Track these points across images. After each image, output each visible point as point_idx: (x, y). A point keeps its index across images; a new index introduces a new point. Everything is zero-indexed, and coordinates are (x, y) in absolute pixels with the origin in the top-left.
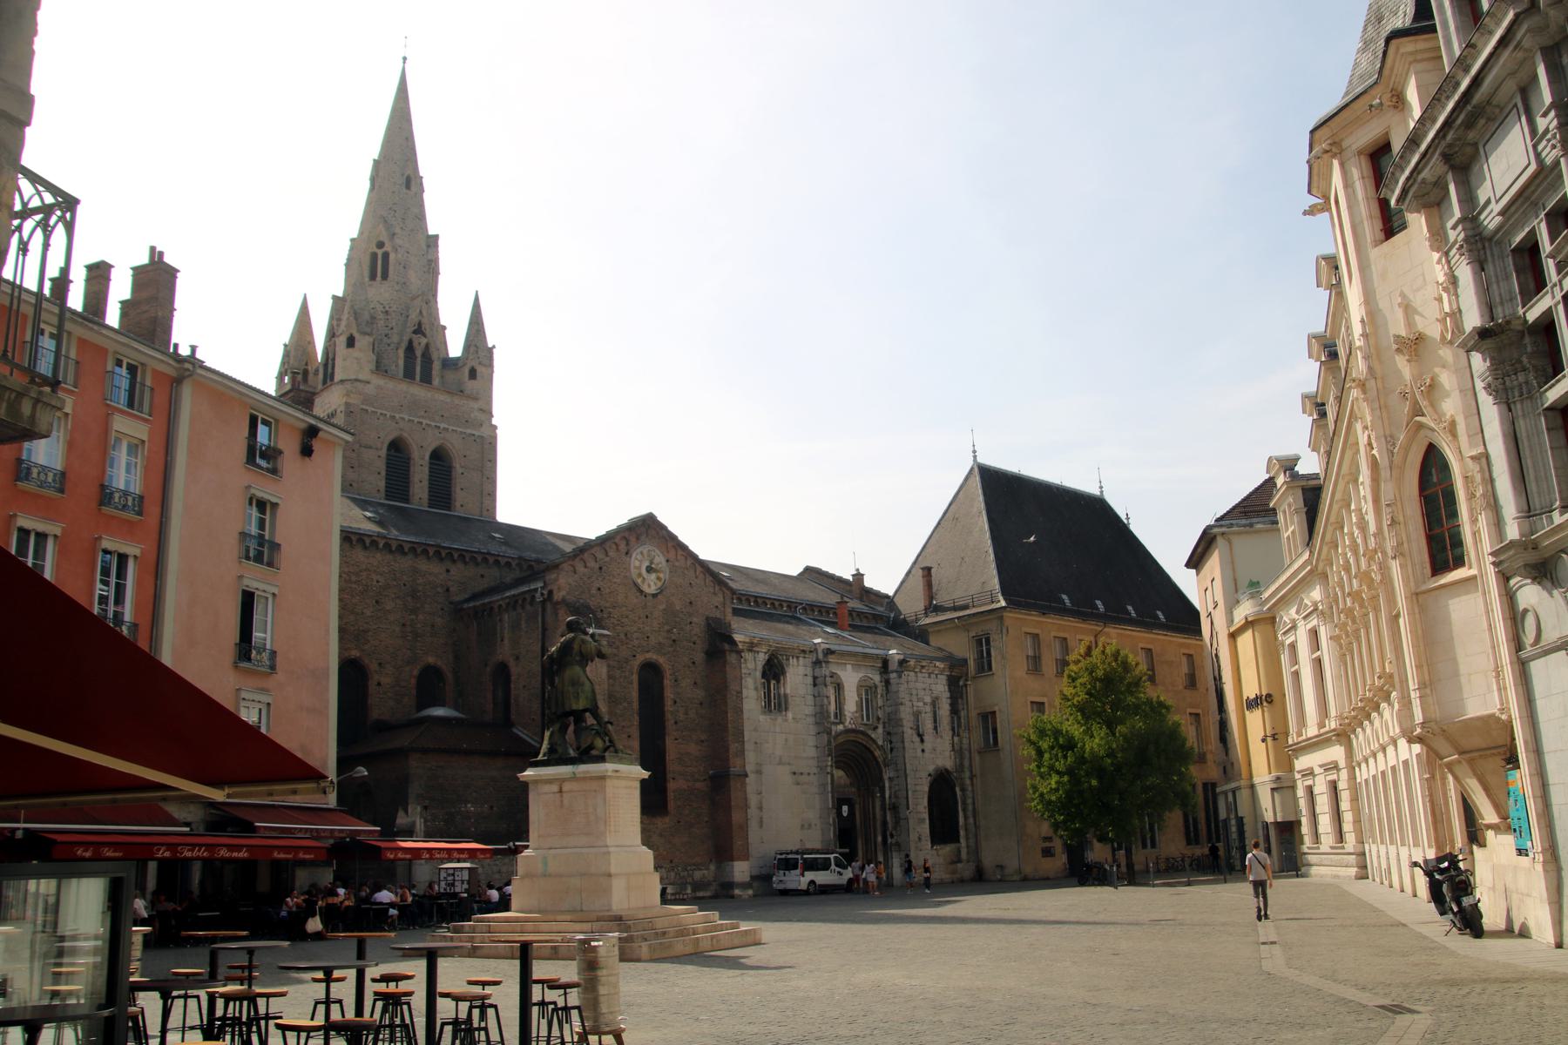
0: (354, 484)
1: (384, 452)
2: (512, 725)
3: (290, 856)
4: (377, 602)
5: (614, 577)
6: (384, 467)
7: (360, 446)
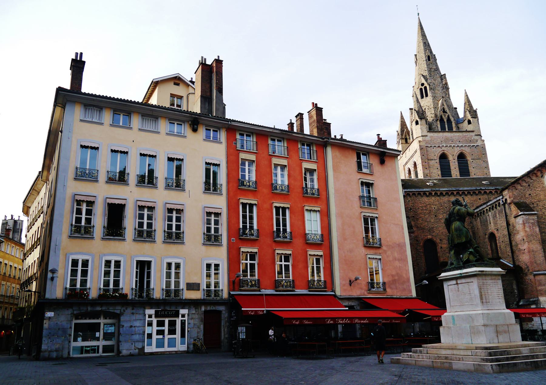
0: (428, 174)
1: (438, 161)
2: (500, 258)
3: (389, 322)
4: (435, 216)
5: (537, 188)
6: (439, 166)
7: (428, 160)
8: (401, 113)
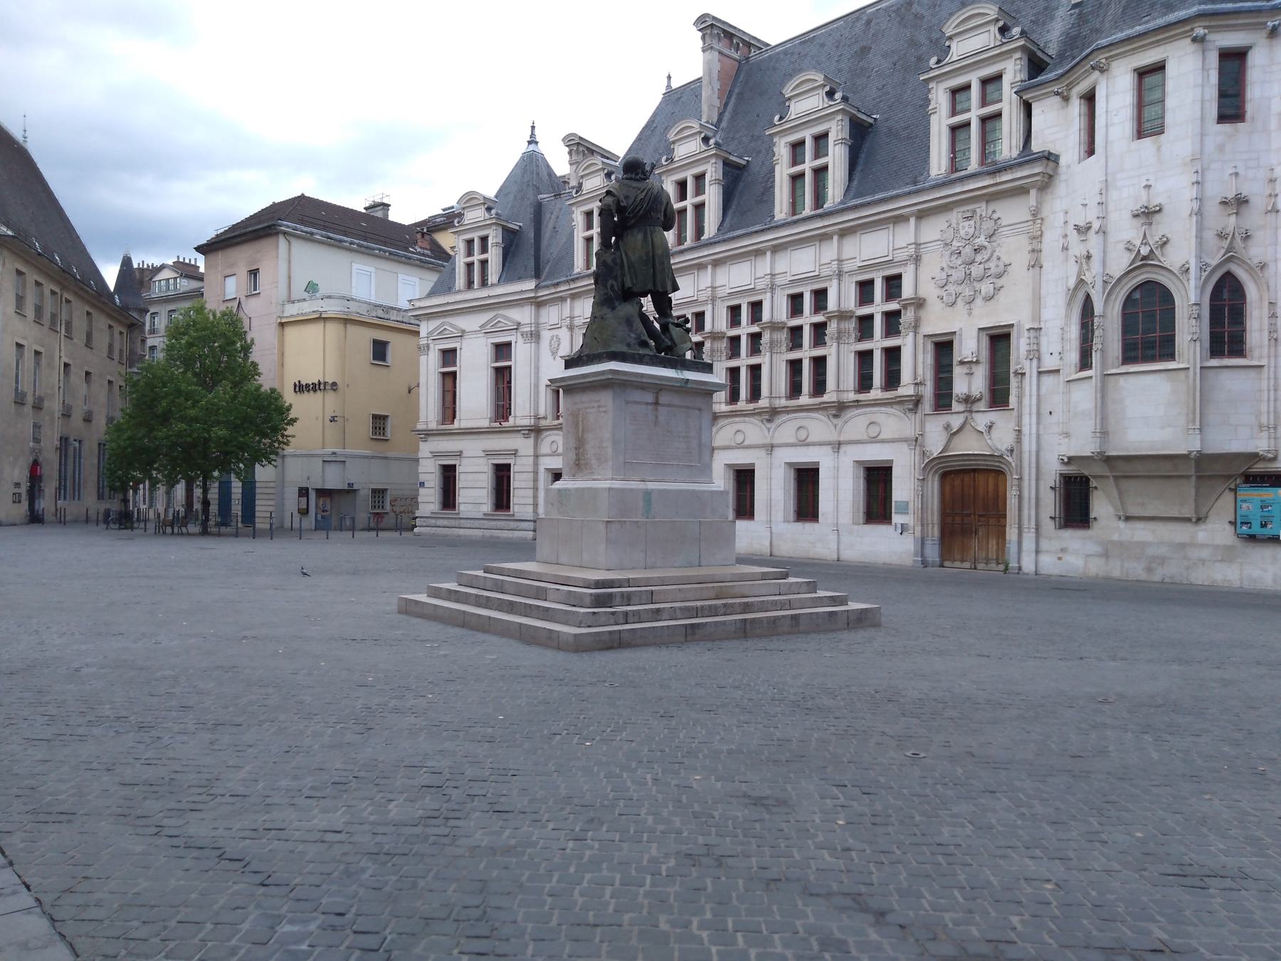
8: (533, 127)
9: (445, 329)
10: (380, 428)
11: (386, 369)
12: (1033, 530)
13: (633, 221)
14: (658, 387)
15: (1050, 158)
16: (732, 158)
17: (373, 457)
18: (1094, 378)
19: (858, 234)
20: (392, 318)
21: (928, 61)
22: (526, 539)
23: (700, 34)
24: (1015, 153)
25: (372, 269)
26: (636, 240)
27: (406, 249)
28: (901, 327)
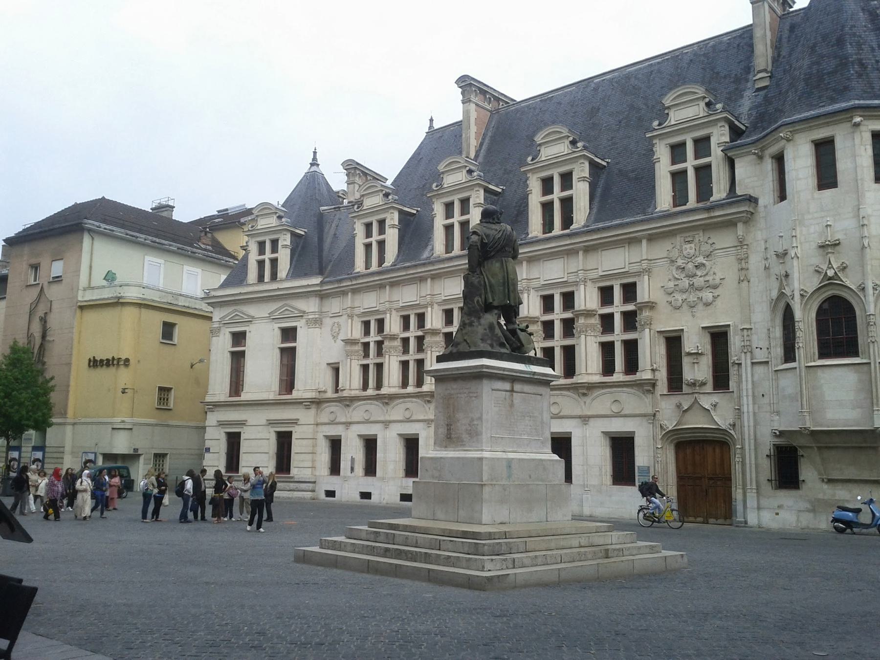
8: (315, 153)
9: (237, 315)
10: (164, 399)
11: (174, 347)
12: (755, 491)
13: (493, 254)
14: (513, 378)
15: (752, 200)
16: (491, 187)
17: (156, 425)
18: (798, 369)
19: (599, 250)
20: (180, 304)
21: (651, 124)
22: (304, 498)
23: (460, 90)
24: (724, 195)
25: (162, 261)
26: (495, 266)
27: (191, 245)
28: (637, 324)
